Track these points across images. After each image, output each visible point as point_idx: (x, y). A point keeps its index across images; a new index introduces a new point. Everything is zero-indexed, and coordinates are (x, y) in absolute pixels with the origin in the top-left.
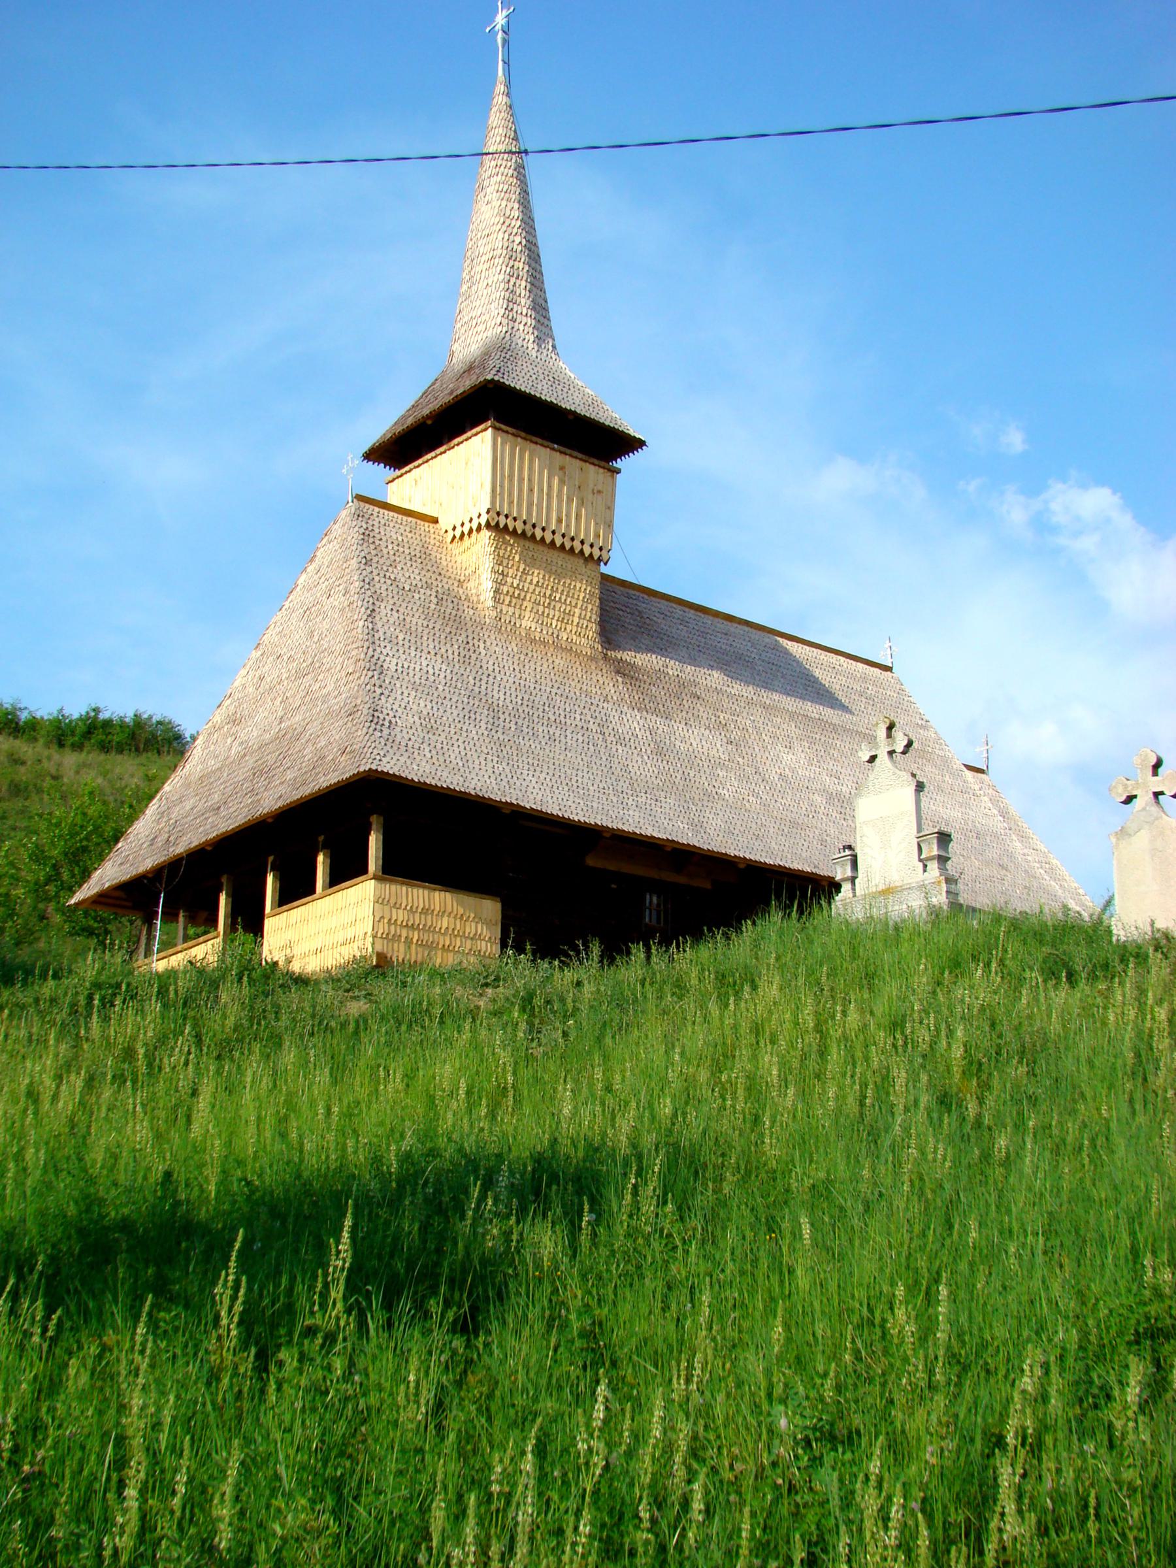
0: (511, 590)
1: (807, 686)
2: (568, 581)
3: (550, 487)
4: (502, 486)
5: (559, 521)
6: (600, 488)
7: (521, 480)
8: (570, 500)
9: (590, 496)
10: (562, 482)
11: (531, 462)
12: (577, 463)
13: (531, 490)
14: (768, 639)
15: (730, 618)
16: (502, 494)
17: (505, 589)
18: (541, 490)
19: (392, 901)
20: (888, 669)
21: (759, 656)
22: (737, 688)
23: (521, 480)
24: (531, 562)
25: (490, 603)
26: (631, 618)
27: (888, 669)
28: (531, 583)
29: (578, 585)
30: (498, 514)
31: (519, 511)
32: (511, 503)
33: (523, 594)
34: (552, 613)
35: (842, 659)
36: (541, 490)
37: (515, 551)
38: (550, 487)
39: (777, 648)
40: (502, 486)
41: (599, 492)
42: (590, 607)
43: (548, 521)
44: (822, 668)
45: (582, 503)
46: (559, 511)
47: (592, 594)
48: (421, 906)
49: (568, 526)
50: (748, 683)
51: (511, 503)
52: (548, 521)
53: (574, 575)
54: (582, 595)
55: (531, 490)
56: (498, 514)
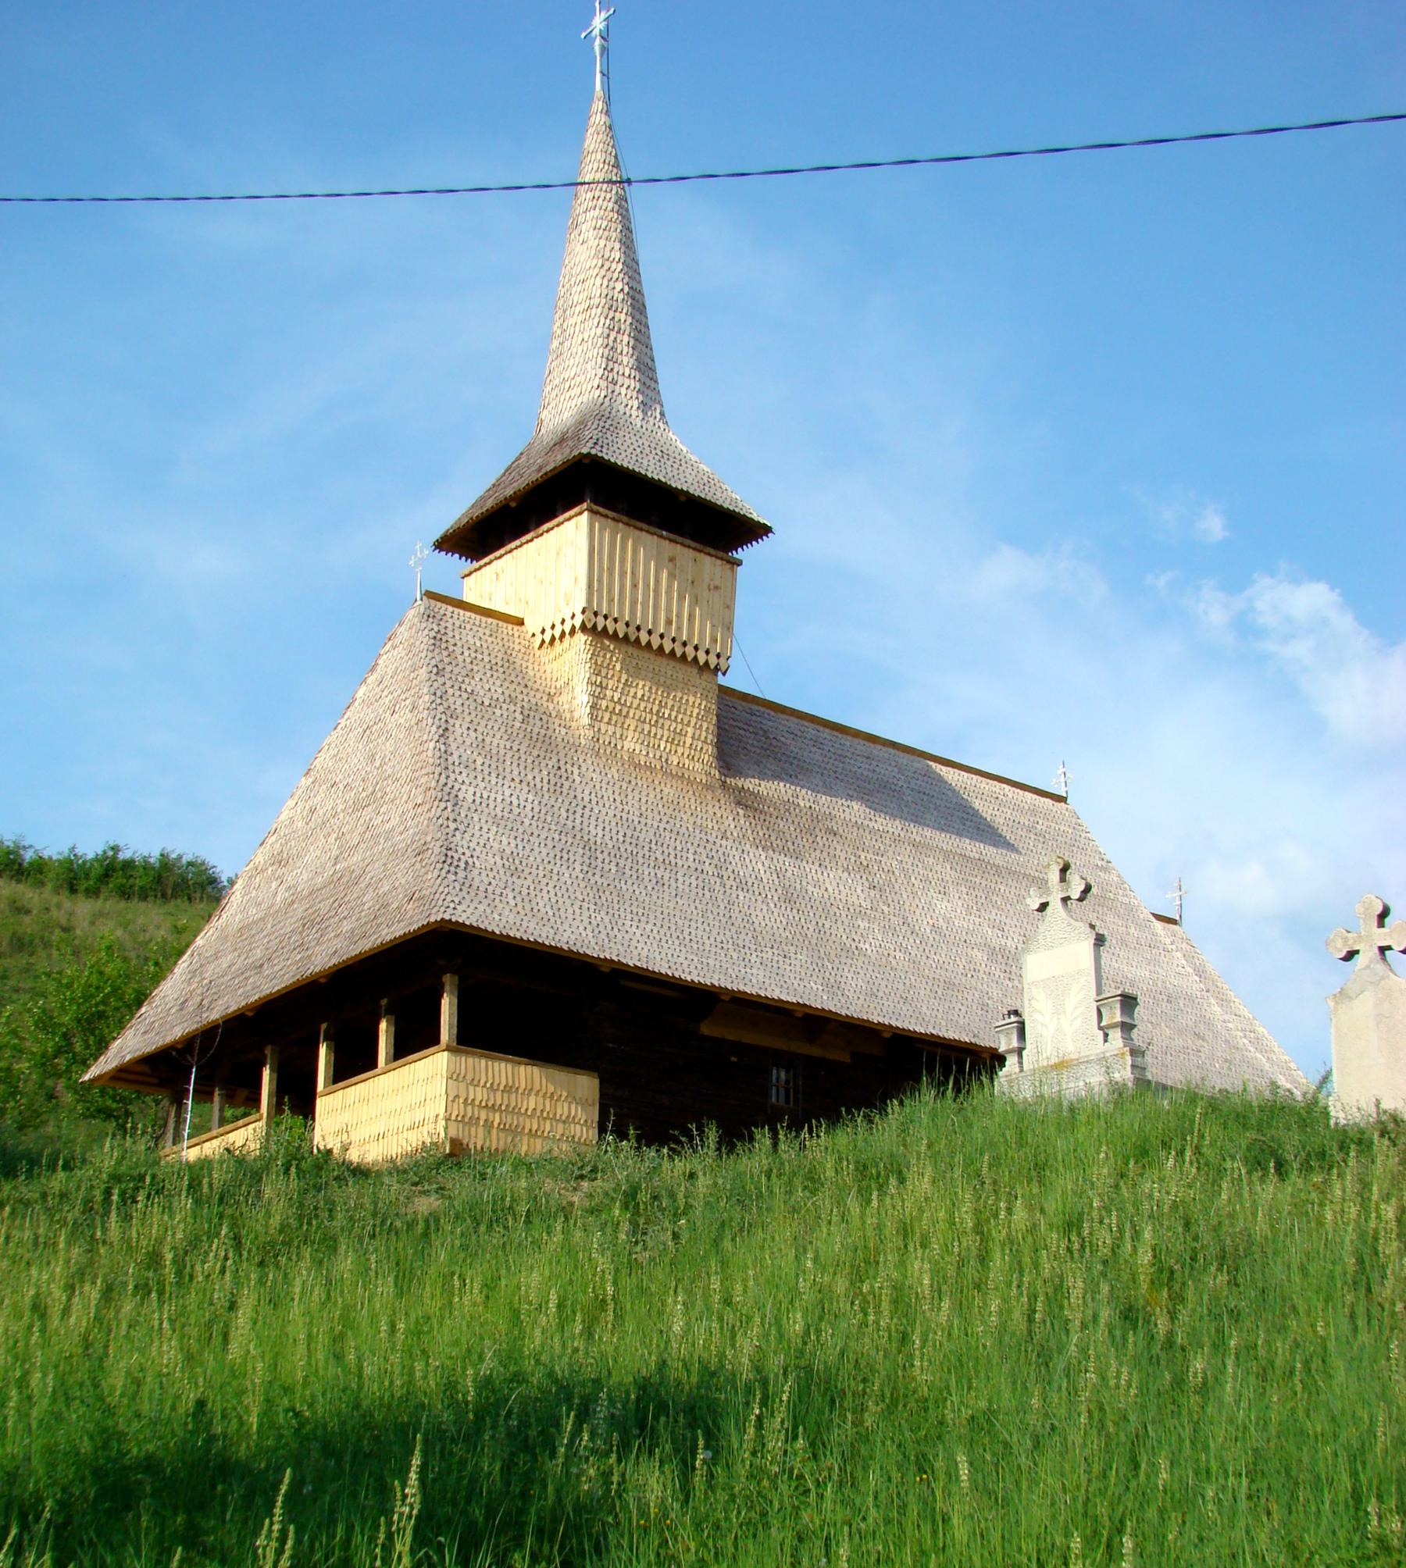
0: (611, 705)
1: (965, 820)
2: (679, 695)
4: (600, 581)
5: (669, 622)
6: (717, 583)
7: (623, 574)
8: (681, 598)
9: (705, 593)
10: (672, 576)
11: (635, 552)
12: (690, 553)
13: (635, 586)
14: (918, 763)
15: (894, 745)
16: (600, 590)
17: (604, 703)
18: (647, 586)
19: (469, 1077)
20: (1062, 799)
21: (907, 785)
22: (881, 822)
23: (623, 574)
24: (635, 672)
25: (586, 721)
26: (754, 739)
27: (1062, 799)
28: (634, 697)
29: (691, 699)
30: (596, 614)
32: (611, 601)
33: (625, 710)
34: (660, 732)
35: (1007, 787)
36: (647, 586)
37: (616, 658)
38: (657, 581)
39: (929, 774)
40: (600, 581)
41: (716, 588)
43: (600, 604)
44: (983, 798)
45: (695, 601)
46: (669, 610)
47: (707, 710)
48: (504, 1083)
49: (679, 628)
50: (894, 816)
51: (611, 601)
53: (686, 686)
54: (696, 711)
55: (635, 586)
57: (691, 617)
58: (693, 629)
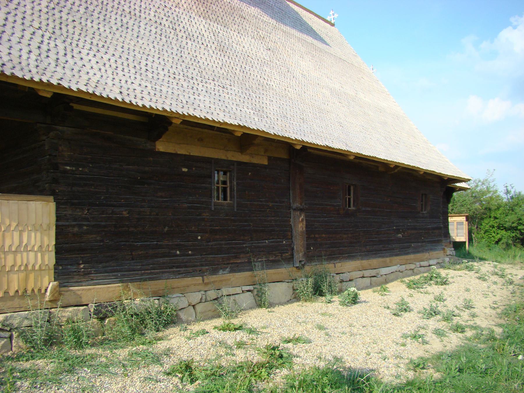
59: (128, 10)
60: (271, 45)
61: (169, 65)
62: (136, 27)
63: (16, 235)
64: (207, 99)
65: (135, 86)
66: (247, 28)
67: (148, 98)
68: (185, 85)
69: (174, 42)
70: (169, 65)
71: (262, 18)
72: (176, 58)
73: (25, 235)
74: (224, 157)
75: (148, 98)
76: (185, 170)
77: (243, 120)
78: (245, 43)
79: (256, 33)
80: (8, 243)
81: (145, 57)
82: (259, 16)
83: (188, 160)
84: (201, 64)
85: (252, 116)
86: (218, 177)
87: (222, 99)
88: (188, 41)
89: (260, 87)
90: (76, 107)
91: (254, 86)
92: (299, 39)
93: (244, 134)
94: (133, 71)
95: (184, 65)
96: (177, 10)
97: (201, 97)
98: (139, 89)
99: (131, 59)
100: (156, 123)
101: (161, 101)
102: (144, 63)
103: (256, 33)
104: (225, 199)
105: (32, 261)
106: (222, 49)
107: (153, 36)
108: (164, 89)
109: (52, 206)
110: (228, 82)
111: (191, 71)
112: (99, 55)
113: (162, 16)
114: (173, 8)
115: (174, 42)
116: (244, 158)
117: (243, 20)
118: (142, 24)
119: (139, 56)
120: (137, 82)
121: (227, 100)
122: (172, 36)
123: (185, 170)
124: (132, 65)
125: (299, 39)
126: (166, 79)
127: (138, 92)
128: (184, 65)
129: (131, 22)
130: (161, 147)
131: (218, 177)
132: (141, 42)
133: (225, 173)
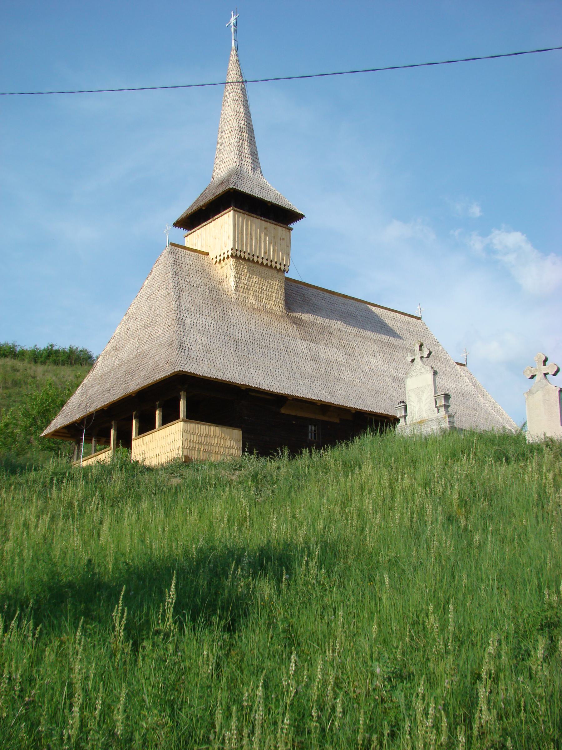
1: (382, 328)
2: (270, 281)
3: (260, 237)
4: (238, 237)
5: (265, 253)
6: (284, 237)
7: (247, 234)
8: (270, 243)
13: (252, 239)
14: (363, 306)
17: (241, 285)
19: (191, 432)
21: (359, 314)
22: (349, 329)
23: (247, 234)
24: (252, 272)
26: (300, 297)
29: (275, 283)
31: (246, 249)
32: (242, 245)
34: (262, 296)
37: (245, 267)
38: (260, 237)
39: (367, 310)
40: (238, 237)
41: (283, 239)
42: (280, 293)
43: (260, 253)
44: (389, 319)
45: (275, 244)
46: (265, 248)
48: (205, 433)
49: (269, 255)
50: (354, 326)
51: (242, 245)
52: (260, 253)
53: (272, 278)
55: (252, 239)
56: (237, 250)
57: (274, 251)
58: (274, 255)
59: (264, 345)
60: (349, 351)
61: (285, 373)
62: (269, 353)
63: (229, 442)
64: (304, 388)
65: (273, 384)
66: (333, 341)
67: (278, 389)
68: (294, 382)
69: (287, 359)
70: (285, 373)
71: (345, 330)
72: (289, 368)
73: (232, 442)
74: (314, 418)
75: (278, 389)
76: (294, 422)
77: (321, 397)
78: (330, 353)
79: (339, 343)
80: (226, 444)
81: (275, 370)
82: (343, 329)
83: (296, 418)
84: (302, 370)
85: (327, 396)
86: (312, 428)
87: (311, 388)
88: (295, 357)
89: (336, 380)
90: (250, 393)
91: (332, 380)
92: (375, 341)
93: (322, 404)
94: (271, 377)
95: (293, 372)
96: (288, 338)
97: (301, 388)
98: (274, 385)
99: (269, 371)
100: (281, 400)
101: (283, 390)
102: (275, 373)
103: (339, 343)
104: (315, 439)
105: (234, 453)
106: (314, 359)
107: (277, 357)
108: (285, 385)
109: (241, 432)
110: (316, 379)
111: (296, 374)
112: (257, 371)
113: (281, 344)
114: (286, 338)
115: (287, 359)
116: (325, 418)
117: (330, 335)
118: (271, 351)
119: (272, 370)
120: (273, 382)
121: (314, 388)
122: (286, 356)
123: (294, 422)
124: (270, 375)
125: (375, 341)
126: (285, 380)
127: (274, 386)
128: (293, 372)
129: (266, 351)
130: (283, 411)
131: (312, 428)
132: (272, 362)
133: (315, 426)
